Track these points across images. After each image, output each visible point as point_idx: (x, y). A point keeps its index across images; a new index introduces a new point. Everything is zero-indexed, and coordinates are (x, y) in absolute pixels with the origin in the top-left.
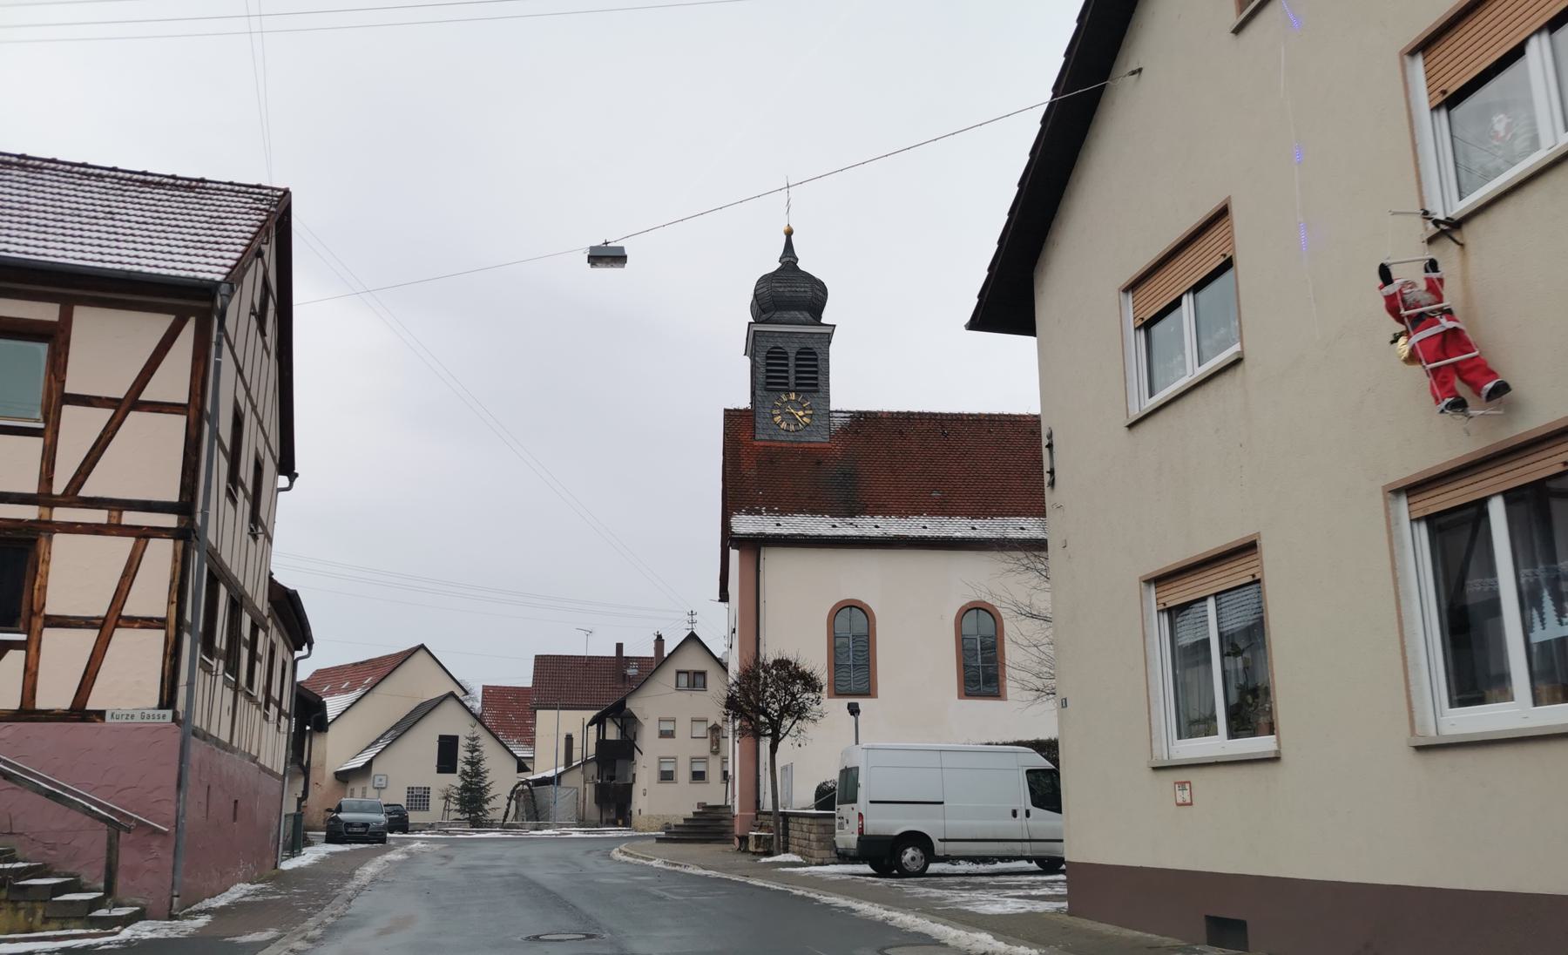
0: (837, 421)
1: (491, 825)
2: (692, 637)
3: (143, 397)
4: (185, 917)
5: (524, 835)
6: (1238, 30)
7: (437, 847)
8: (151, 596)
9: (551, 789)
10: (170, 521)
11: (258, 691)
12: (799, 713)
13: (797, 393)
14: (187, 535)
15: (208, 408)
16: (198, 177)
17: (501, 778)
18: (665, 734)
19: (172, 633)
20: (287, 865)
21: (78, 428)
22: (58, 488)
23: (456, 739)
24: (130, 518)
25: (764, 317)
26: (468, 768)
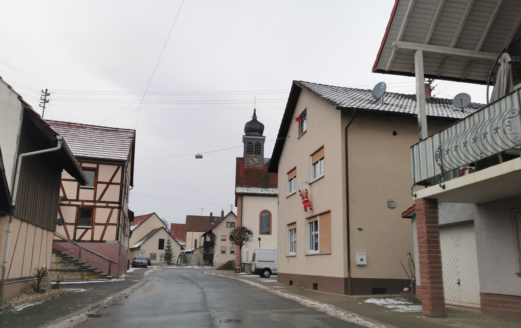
0: (266, 161)
1: (173, 264)
5: (183, 267)
8: (114, 219)
9: (190, 255)
10: (117, 205)
12: (247, 240)
14: (120, 208)
17: (176, 251)
18: (223, 240)
20: (128, 272)
21: (101, 188)
22: (97, 199)
23: (164, 240)
24: (110, 205)
26: (167, 248)
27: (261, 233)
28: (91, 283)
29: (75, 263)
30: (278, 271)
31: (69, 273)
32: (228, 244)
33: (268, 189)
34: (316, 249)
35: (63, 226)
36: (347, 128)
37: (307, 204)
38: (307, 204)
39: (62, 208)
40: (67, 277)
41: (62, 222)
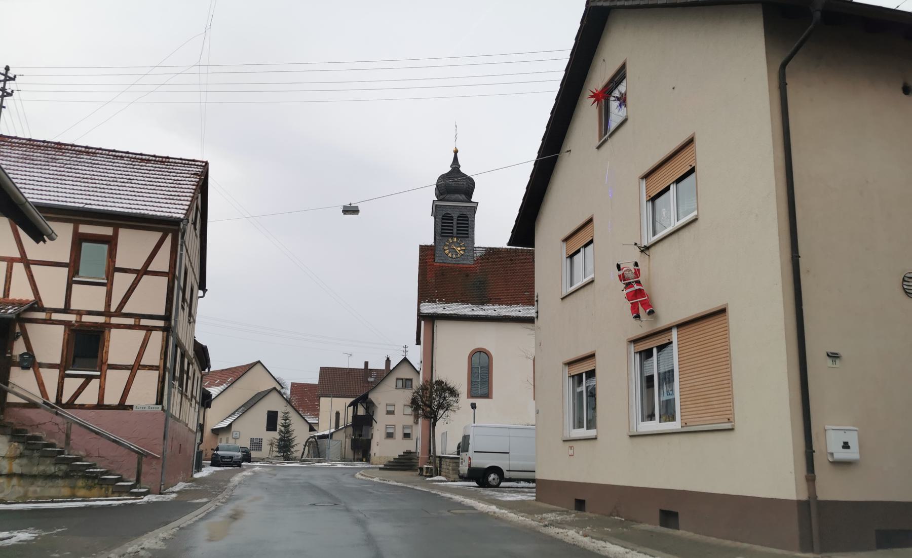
0: (478, 253)
1: (294, 460)
2: (405, 360)
3: (149, 269)
4: (165, 494)
5: (312, 465)
6: (598, 147)
7: (267, 470)
8: (153, 356)
9: (327, 441)
10: (161, 323)
11: (189, 394)
12: (447, 407)
13: (457, 237)
14: (168, 330)
15: (177, 273)
16: (165, 155)
17: (300, 435)
18: (390, 413)
19: (162, 372)
20: (197, 476)
21: (122, 282)
23: (276, 413)
24: (144, 322)
25: (441, 197)
26: (283, 429)
27: (471, 395)
28: (91, 507)
29: (57, 457)
30: (538, 476)
31: (40, 482)
32: (403, 418)
33: (485, 307)
34: (673, 418)
35: (31, 371)
36: (784, 66)
37: (639, 299)
38: (639, 299)
39: (31, 328)
40: (35, 492)
41: (29, 362)
